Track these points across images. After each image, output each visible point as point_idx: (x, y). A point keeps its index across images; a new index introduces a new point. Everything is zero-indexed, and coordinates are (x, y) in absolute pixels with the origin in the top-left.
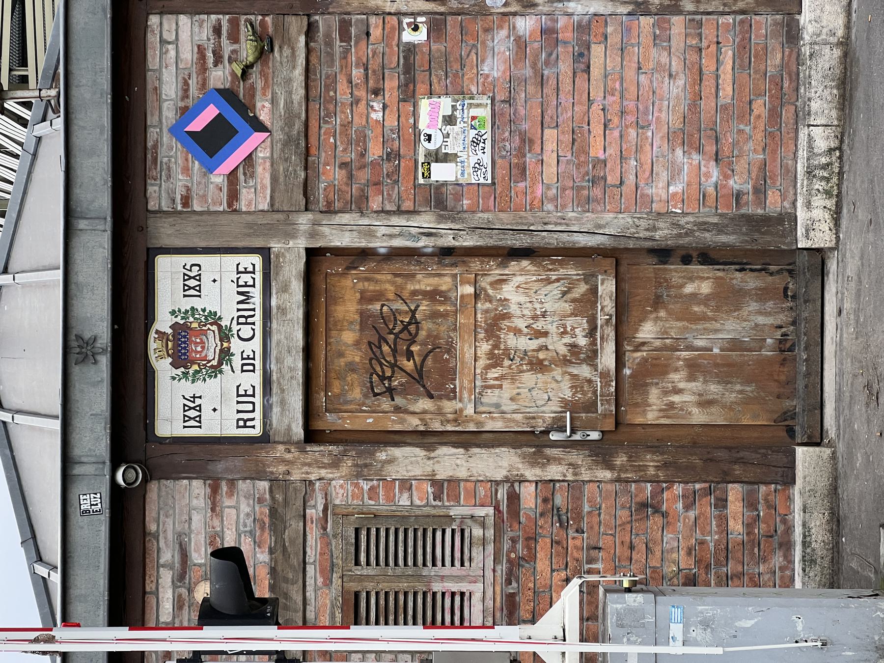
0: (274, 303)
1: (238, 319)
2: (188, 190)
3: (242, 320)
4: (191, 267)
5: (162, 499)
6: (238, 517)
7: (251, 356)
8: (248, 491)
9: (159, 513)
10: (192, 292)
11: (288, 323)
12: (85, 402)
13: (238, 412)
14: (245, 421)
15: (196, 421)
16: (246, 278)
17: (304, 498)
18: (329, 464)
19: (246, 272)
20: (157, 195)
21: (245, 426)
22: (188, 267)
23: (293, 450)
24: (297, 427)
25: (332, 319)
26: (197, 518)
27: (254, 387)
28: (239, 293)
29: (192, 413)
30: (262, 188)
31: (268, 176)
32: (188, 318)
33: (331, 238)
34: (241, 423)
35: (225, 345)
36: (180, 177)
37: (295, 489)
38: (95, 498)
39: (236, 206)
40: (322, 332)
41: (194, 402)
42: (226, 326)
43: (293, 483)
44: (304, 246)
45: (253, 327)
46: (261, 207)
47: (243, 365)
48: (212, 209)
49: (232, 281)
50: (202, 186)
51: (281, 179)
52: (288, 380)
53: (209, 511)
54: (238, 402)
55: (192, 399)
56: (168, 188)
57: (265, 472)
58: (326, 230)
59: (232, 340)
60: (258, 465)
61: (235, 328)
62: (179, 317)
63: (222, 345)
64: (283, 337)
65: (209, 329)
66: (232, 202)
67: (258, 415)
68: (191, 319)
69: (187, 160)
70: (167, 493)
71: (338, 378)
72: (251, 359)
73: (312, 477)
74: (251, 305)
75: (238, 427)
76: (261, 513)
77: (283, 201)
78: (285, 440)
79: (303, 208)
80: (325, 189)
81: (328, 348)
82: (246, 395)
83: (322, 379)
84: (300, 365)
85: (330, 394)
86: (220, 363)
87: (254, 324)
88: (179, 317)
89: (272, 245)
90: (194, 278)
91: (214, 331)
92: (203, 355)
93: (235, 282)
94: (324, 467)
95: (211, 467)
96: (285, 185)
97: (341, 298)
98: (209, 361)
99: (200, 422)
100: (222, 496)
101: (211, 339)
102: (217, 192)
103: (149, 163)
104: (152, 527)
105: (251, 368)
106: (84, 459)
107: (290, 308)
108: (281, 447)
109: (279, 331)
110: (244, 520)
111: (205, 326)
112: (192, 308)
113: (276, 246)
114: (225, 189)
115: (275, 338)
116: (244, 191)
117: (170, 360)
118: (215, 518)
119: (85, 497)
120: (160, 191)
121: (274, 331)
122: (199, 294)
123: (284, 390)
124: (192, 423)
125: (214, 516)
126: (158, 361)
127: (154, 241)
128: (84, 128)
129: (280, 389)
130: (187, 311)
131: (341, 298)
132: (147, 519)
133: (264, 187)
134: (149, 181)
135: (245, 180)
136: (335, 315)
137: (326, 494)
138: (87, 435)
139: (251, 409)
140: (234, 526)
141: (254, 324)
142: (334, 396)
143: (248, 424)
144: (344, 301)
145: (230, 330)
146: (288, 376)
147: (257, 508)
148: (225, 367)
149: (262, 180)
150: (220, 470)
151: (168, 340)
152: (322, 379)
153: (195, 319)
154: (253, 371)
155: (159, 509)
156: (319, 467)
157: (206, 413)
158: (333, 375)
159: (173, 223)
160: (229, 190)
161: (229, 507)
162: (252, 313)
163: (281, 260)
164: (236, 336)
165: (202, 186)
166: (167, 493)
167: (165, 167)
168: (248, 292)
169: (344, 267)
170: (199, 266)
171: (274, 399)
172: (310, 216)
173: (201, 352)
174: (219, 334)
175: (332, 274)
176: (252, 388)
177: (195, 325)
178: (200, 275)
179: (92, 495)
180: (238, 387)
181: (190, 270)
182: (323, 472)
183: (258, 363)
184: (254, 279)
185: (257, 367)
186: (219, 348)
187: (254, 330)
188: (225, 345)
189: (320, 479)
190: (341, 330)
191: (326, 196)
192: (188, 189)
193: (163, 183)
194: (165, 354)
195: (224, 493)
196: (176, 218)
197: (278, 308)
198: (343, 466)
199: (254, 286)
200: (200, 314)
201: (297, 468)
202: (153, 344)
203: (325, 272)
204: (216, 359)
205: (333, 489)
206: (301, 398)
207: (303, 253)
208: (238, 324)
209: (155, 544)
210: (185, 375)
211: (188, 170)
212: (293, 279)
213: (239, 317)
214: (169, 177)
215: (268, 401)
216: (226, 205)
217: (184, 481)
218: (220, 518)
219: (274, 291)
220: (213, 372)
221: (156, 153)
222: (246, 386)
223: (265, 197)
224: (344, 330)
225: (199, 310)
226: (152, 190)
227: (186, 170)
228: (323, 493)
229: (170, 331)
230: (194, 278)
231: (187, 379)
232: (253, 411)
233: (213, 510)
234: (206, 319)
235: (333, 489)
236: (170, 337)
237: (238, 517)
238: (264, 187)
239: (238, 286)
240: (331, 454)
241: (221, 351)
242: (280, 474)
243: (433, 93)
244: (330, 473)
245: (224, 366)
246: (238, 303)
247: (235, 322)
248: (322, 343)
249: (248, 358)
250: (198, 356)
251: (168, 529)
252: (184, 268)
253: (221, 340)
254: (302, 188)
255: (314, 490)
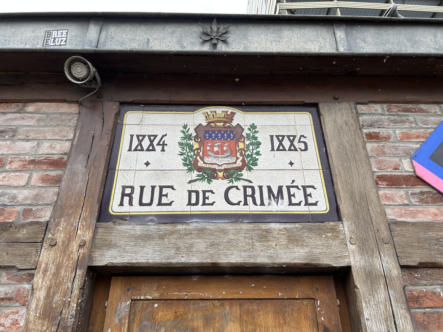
0: (273, 226)
1: (250, 187)
2: (386, 138)
3: (249, 191)
4: (302, 142)
5: (58, 116)
6: (16, 187)
7: (207, 201)
8: (43, 198)
9: (44, 114)
10: (276, 143)
11: (249, 244)
12: (162, 35)
13: (142, 188)
14: (130, 196)
15: (137, 146)
16: (299, 196)
17: (13, 267)
18: (51, 303)
19: (306, 196)
20: (373, 112)
21: (123, 195)
22: (303, 139)
23: (81, 251)
24: (112, 257)
25: (255, 308)
26: (28, 146)
27: (170, 204)
28: (280, 189)
29: (146, 143)
30: (412, 212)
31: (428, 218)
32: (249, 140)
33: (372, 303)
34: (128, 191)
35: (221, 174)
36: (398, 132)
37: (28, 255)
38: (62, 41)
39: (383, 184)
40: (238, 293)
41: (158, 144)
42: (242, 175)
43: (37, 252)
44: (353, 264)
45: (242, 204)
46: (388, 211)
47: (197, 193)
48: (372, 161)
49: (293, 181)
50: (394, 151)
51: (431, 234)
52: (175, 244)
53: (32, 158)
54: (153, 188)
55: (161, 143)
56: (383, 122)
57: (61, 216)
58: (381, 294)
59: (226, 181)
60: (71, 208)
61: (240, 184)
62: (249, 132)
63: (220, 171)
64: (231, 237)
65: (237, 158)
66: (385, 180)
67: (136, 209)
68: (247, 142)
69: (418, 137)
70: (63, 121)
71: (176, 317)
72: (204, 201)
73: (38, 279)
74: (268, 201)
75: (124, 188)
76: (10, 214)
77: (405, 236)
78: (97, 241)
79: (404, 262)
80: (435, 293)
81: (217, 303)
82: (161, 195)
83: (175, 294)
84: (195, 259)
85: (156, 305)
86: (200, 169)
87: (246, 204)
88: (249, 132)
89: (345, 223)
90: (292, 144)
91: (235, 163)
92: (209, 153)
93: (293, 184)
94: (48, 296)
95: (82, 158)
96: (426, 239)
97: (284, 320)
98: (202, 159)
99: (136, 150)
100: (45, 170)
101: (226, 160)
102: (392, 165)
103: (404, 106)
104: (31, 108)
105: (193, 201)
106: (103, 34)
107: (268, 246)
108: (88, 236)
109: (238, 232)
110: (9, 194)
111: (241, 154)
112: (259, 144)
113: (346, 229)
114: (396, 173)
115: (229, 227)
116: (402, 192)
117: (204, 124)
118: (21, 163)
119: (64, 33)
120: (378, 114)
121: (237, 226)
122: (275, 149)
123: (163, 239)
124: (135, 143)
125: (24, 163)
126: (204, 114)
127: (326, 108)
128: (436, 36)
129: (165, 235)
130: (256, 138)
131: (284, 320)
132: (41, 104)
133: (413, 214)
134: (385, 105)
135: (415, 194)
136: (261, 312)
137: (10, 299)
138: (128, 37)
139: (144, 201)
140: (6, 183)
141: (246, 204)
142: (153, 313)
143: (126, 199)
144: (281, 326)
145: (238, 179)
146: (180, 243)
147: (19, 208)
148: (195, 174)
149: (422, 212)
150: (75, 167)
151: (225, 122)
152: (175, 294)
153: (248, 146)
154: (190, 204)
155: (48, 114)
156: (49, 288)
157: (144, 156)
158: (181, 310)
159: (349, 124)
160: (398, 177)
161: (30, 178)
162: (258, 201)
163: (329, 235)
164: (231, 184)
165: (394, 151)
166: (63, 121)
167: (404, 118)
168: (282, 198)
169: (326, 324)
170: (306, 149)
171: (153, 228)
172: (395, 271)
173: (213, 151)
174: (233, 168)
175: (314, 307)
176: (169, 202)
177: (241, 145)
178: (296, 150)
179: (65, 39)
180: (172, 187)
181: (299, 142)
182: (41, 294)
183: (199, 209)
184: (299, 204)
185: (194, 208)
186: (217, 167)
187: (238, 204)
188: (221, 174)
189: (33, 289)
190: (241, 321)
191: (425, 295)
192: (387, 138)
193: (387, 117)
194: (211, 120)
195: (48, 173)
196: (354, 126)
197: (268, 231)
198: (43, 326)
199: (291, 204)
200: (253, 150)
201: (56, 258)
202: (220, 111)
203: (317, 297)
204: (204, 165)
205: (15, 310)
206: (151, 261)
207: (342, 263)
208: (245, 188)
209: (13, 111)
210: (189, 137)
211: (408, 139)
212: (307, 250)
213: (253, 188)
214: (395, 122)
215: (152, 221)
216: (380, 174)
217: (72, 135)
218: (19, 169)
219: (288, 226)
220: (190, 162)
221: (415, 112)
222: (172, 195)
223: (401, 216)
224: (241, 325)
225: (258, 150)
226: (378, 108)
227: (407, 137)
228: (14, 295)
229: (234, 123)
230: (292, 144)
231: (184, 138)
232: (141, 204)
233: (32, 162)
234: (248, 156)
235: (15, 310)
236: (228, 125)
237: (16, 187)
238: (413, 214)
239: (288, 188)
240: (64, 305)
241: (214, 170)
242: (53, 235)
243: (133, 302)
244: (37, 305)
245: (196, 173)
246: (269, 188)
247: (247, 184)
248: (224, 294)
249: (205, 198)
250: (208, 148)
251: (24, 121)
252: (301, 136)
253: (226, 170)
254: (428, 260)
255: (20, 281)
